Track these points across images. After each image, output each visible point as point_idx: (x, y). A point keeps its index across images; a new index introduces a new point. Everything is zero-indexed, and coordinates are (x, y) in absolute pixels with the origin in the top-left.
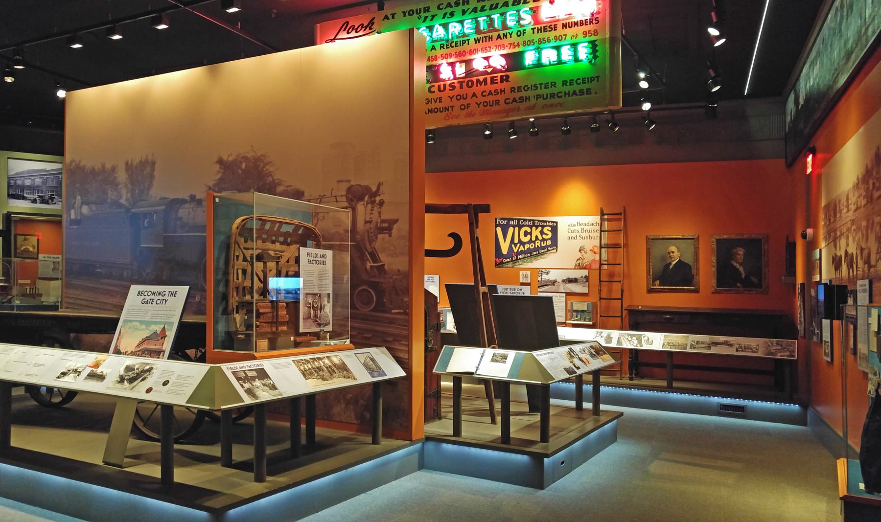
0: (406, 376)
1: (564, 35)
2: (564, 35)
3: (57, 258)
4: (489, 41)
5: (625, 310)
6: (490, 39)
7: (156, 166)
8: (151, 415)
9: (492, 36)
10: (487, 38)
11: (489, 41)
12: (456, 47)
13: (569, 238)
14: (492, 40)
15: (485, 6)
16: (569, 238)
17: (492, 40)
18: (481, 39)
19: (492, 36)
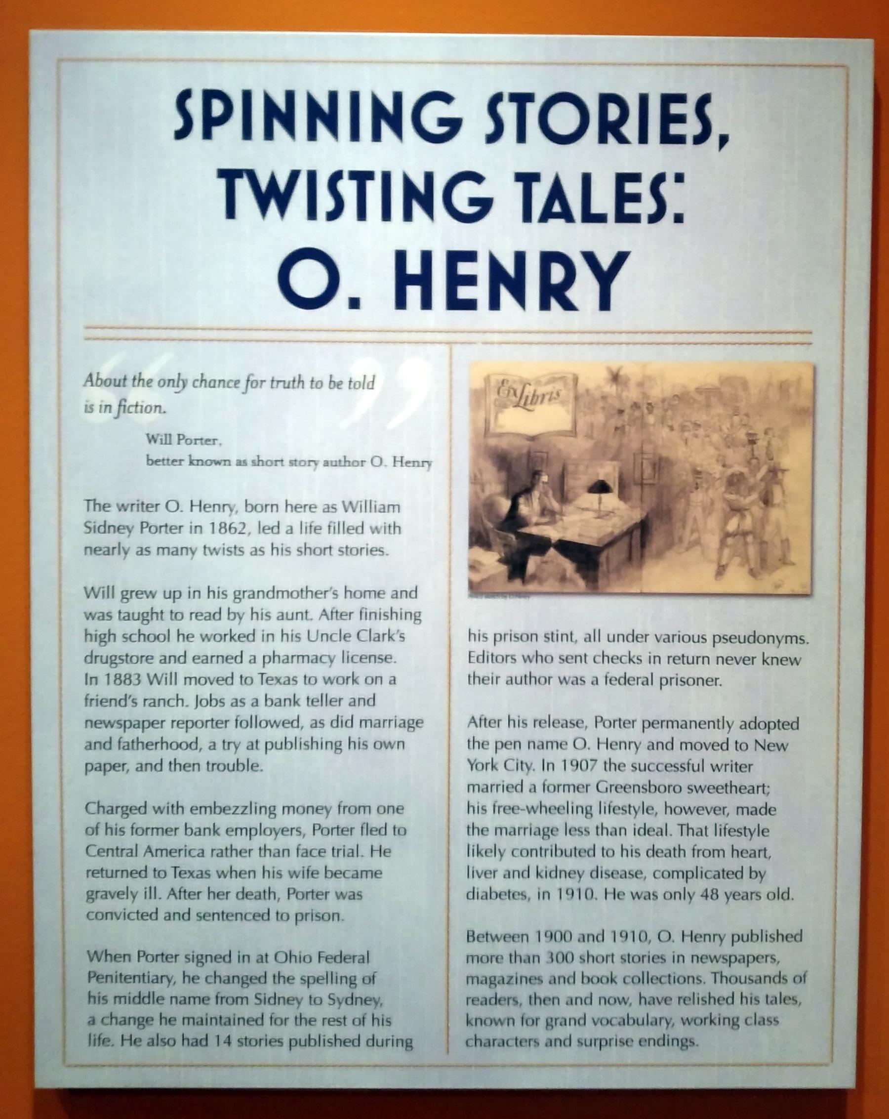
1: (601, 218)
2: (601, 218)
4: (426, 258)
6: (414, 267)
9: (401, 302)
10: (374, 189)
11: (426, 258)
12: (622, 217)
14: (401, 257)
17: (401, 257)
19: (401, 302)
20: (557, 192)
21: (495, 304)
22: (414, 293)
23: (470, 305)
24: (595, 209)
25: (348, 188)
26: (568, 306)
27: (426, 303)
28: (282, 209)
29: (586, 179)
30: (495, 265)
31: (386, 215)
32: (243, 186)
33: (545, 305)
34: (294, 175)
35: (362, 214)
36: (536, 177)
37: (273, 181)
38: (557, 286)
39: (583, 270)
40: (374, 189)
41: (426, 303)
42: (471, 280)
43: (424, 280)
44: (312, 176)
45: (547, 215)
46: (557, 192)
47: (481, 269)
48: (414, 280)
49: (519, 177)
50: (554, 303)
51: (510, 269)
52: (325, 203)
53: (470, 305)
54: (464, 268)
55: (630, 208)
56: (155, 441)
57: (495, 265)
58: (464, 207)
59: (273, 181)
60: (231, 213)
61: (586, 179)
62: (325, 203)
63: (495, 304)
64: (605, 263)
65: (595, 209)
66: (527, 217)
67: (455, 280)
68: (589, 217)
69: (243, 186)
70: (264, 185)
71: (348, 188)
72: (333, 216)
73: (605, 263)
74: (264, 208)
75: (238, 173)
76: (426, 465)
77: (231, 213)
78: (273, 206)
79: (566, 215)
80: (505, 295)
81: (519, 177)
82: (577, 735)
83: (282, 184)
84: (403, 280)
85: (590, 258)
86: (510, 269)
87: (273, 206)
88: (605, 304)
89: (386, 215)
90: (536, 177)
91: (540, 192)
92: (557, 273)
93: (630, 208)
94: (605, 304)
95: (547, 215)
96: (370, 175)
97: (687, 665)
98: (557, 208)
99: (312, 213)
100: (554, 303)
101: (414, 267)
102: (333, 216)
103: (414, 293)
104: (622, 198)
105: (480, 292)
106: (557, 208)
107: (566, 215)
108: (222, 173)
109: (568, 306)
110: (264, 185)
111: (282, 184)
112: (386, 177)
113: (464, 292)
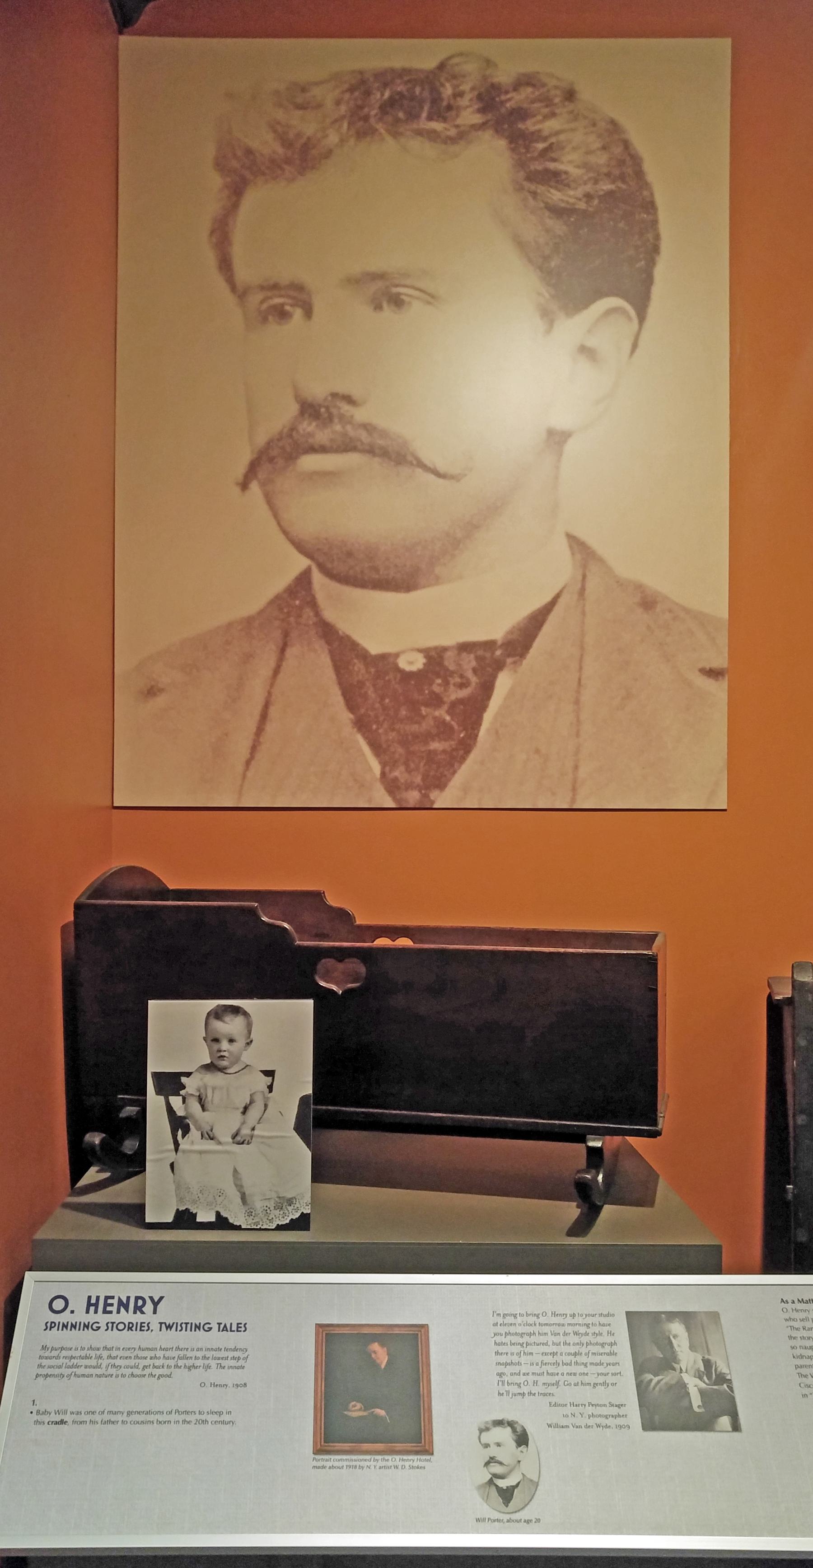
0: (111, 1175)
1: (234, 1331)
2: (234, 1331)
3: (53, 1367)
4: (98, 1298)
5: (430, 1458)
6: (93, 1301)
7: (688, 1344)
8: (283, 650)
9: (88, 1312)
10: (189, 1326)
11: (98, 1298)
12: (238, 1331)
13: (241, 1327)
14: (90, 1298)
15: (261, 1071)
16: (241, 1327)
17: (90, 1298)
18: (175, 1325)
19: (88, 1312)
20: (225, 1326)
21: (118, 1312)
22: (92, 1309)
23: (111, 1312)
24: (233, 1329)
25: (184, 1326)
26: (143, 1313)
27: (96, 1312)
28: (171, 1330)
29: (231, 1324)
30: (120, 1300)
31: (191, 1330)
32: (163, 1325)
33: (135, 1312)
34: (173, 1324)
35: (186, 1330)
36: (221, 1323)
37: (169, 1325)
38: (140, 1307)
39: (148, 1301)
40: (189, 1326)
41: (96, 1312)
42: (112, 1305)
43: (96, 1305)
44: (177, 1323)
45: (223, 1330)
46: (225, 1326)
47: (115, 1302)
48: (93, 1305)
49: (218, 1323)
50: (138, 1312)
51: (125, 1301)
52: (179, 1328)
53: (111, 1312)
54: (110, 1301)
55: (239, 1329)
56: (551, 1427)
57: (120, 1300)
58: (206, 1329)
59: (169, 1325)
60: (161, 1330)
61: (231, 1324)
62: (179, 1328)
63: (118, 1312)
64: (156, 1300)
65: (233, 1329)
66: (219, 1331)
67: (106, 1305)
68: (231, 1331)
69: (163, 1325)
70: (167, 1325)
71: (184, 1326)
72: (181, 1330)
73: (156, 1300)
74: (167, 1329)
75: (162, 1323)
76: (225, 1386)
77: (161, 1330)
78: (169, 1329)
79: (227, 1330)
80: (122, 1309)
81: (218, 1323)
82: (784, 1307)
83: (171, 1325)
84: (89, 1304)
85: (151, 1298)
86: (125, 1301)
87: (169, 1329)
88: (155, 1312)
89: (191, 1330)
90: (221, 1323)
91: (222, 1326)
92: (140, 1303)
93: (239, 1329)
94: (155, 1312)
95: (223, 1330)
96: (188, 1323)
97: (225, 1425)
98: (225, 1329)
99: (176, 1330)
100: (138, 1312)
101: (93, 1301)
102: (181, 1330)
103: (92, 1309)
104: (238, 1327)
105: (114, 1309)
106: (225, 1329)
107: (227, 1330)
108: (160, 1323)
109: (143, 1313)
110: (167, 1325)
111: (171, 1325)
112: (192, 1324)
113: (109, 1309)
